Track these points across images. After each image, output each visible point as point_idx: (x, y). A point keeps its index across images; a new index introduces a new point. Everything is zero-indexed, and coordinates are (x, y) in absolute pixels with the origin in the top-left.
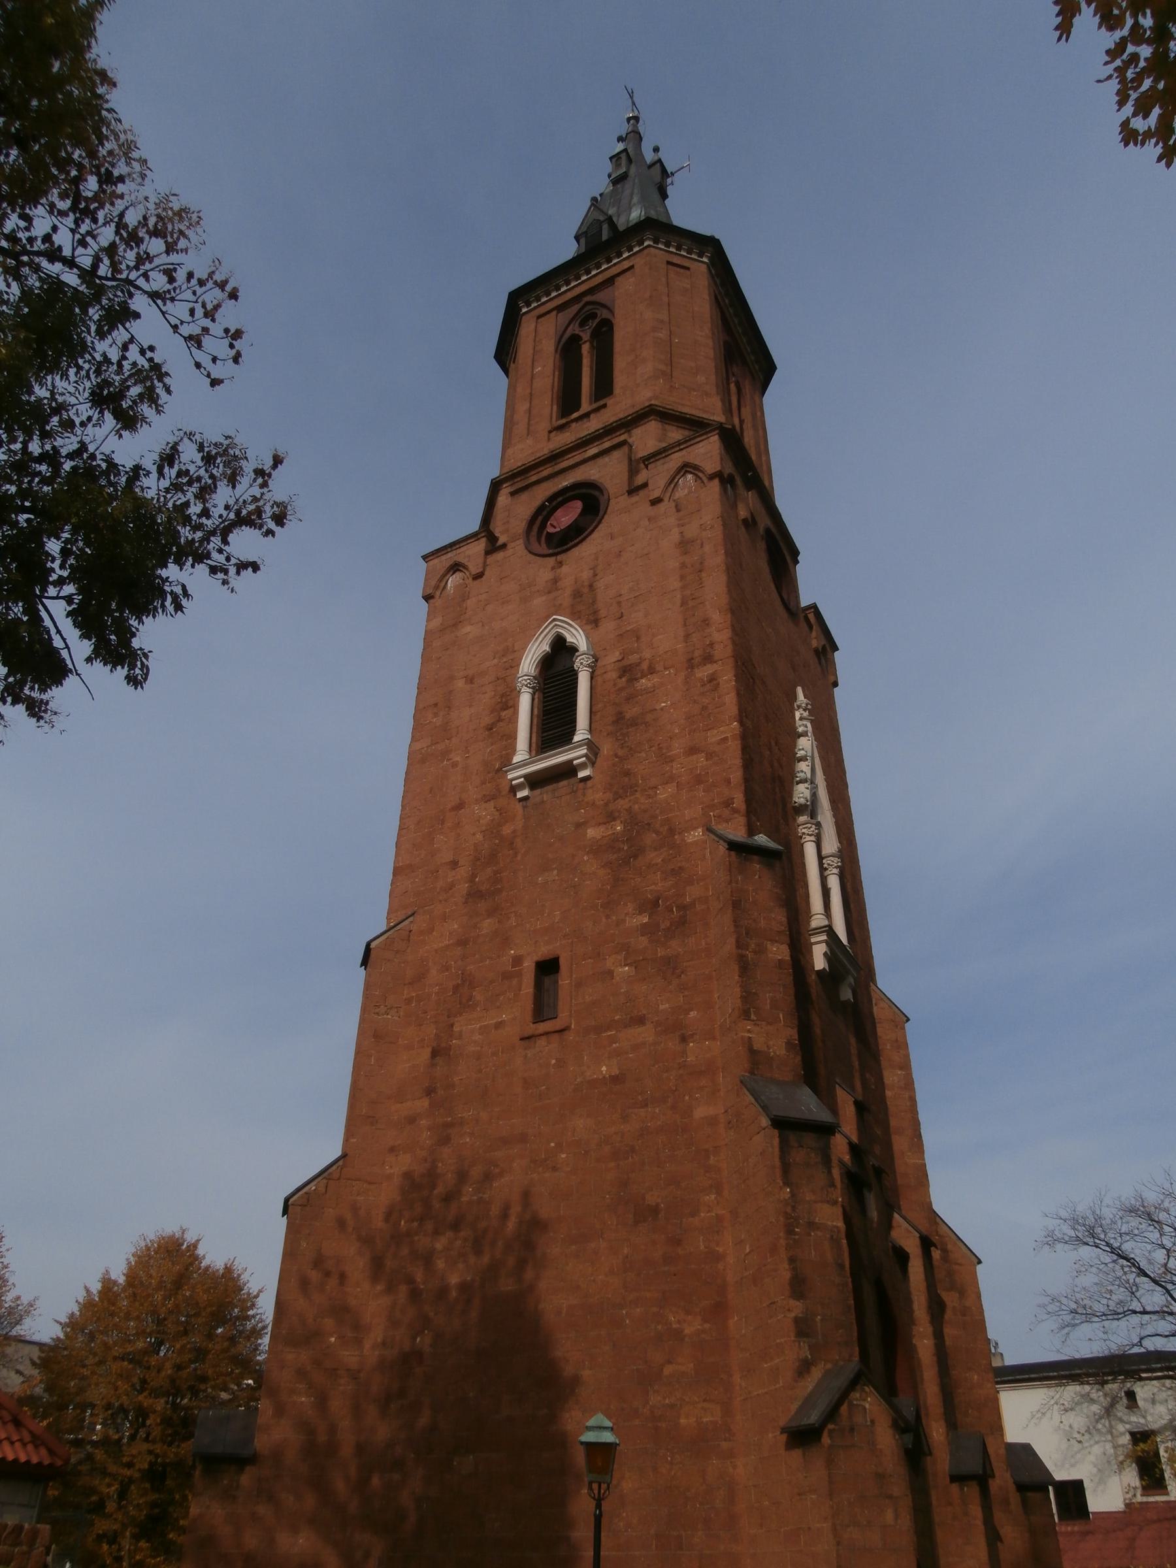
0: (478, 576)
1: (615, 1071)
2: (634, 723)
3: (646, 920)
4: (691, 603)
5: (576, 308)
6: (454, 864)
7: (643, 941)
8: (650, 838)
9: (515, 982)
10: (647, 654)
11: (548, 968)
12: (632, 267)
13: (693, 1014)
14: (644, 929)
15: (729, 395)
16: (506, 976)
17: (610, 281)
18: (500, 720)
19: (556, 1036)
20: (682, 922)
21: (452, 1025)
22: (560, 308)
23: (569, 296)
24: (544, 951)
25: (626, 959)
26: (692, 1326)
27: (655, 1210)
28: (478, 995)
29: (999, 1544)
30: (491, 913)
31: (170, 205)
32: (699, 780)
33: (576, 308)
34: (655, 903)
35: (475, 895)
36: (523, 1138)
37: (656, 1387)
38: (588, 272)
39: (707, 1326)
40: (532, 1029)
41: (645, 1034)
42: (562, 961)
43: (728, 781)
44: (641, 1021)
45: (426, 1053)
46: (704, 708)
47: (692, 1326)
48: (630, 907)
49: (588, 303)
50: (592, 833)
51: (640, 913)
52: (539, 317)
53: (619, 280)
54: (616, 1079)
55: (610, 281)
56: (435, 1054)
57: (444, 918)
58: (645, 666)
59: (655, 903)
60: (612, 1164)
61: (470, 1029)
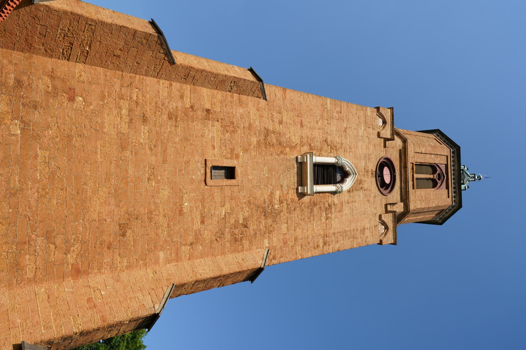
0: (379, 135)
1: (185, 210)
2: (312, 211)
3: (240, 222)
4: (344, 234)
5: (444, 171)
6: (281, 122)
7: (232, 221)
8: (270, 221)
9: (229, 155)
10: (333, 216)
11: (230, 173)
12: (449, 197)
13: (201, 247)
14: (237, 221)
15: (406, 172)
16: (232, 150)
17: (447, 188)
18: (328, 145)
19: (204, 178)
20: (236, 240)
21: (218, 121)
22: (447, 166)
23: (449, 170)
24: (238, 172)
25: (228, 213)
26: (71, 258)
27: (124, 235)
28: (228, 135)
29: (84, 332)
30: (258, 142)
31: (128, 334)
32: (285, 243)
33: (444, 171)
34: (246, 226)
35: (267, 133)
36: (164, 161)
37: (45, 241)
38: (454, 179)
39: (70, 267)
40: (209, 165)
41: (197, 225)
42: (233, 181)
43: (281, 257)
44: (203, 222)
45: (208, 106)
46: (309, 243)
47: (71, 258)
48: (246, 214)
49: (444, 177)
50: (278, 193)
51: (244, 219)
52: (447, 156)
53: (447, 191)
54: (181, 211)
55: (447, 188)
56: (208, 111)
57: (261, 116)
58: (329, 215)
59: (246, 226)
60: (146, 211)
61: (213, 131)
